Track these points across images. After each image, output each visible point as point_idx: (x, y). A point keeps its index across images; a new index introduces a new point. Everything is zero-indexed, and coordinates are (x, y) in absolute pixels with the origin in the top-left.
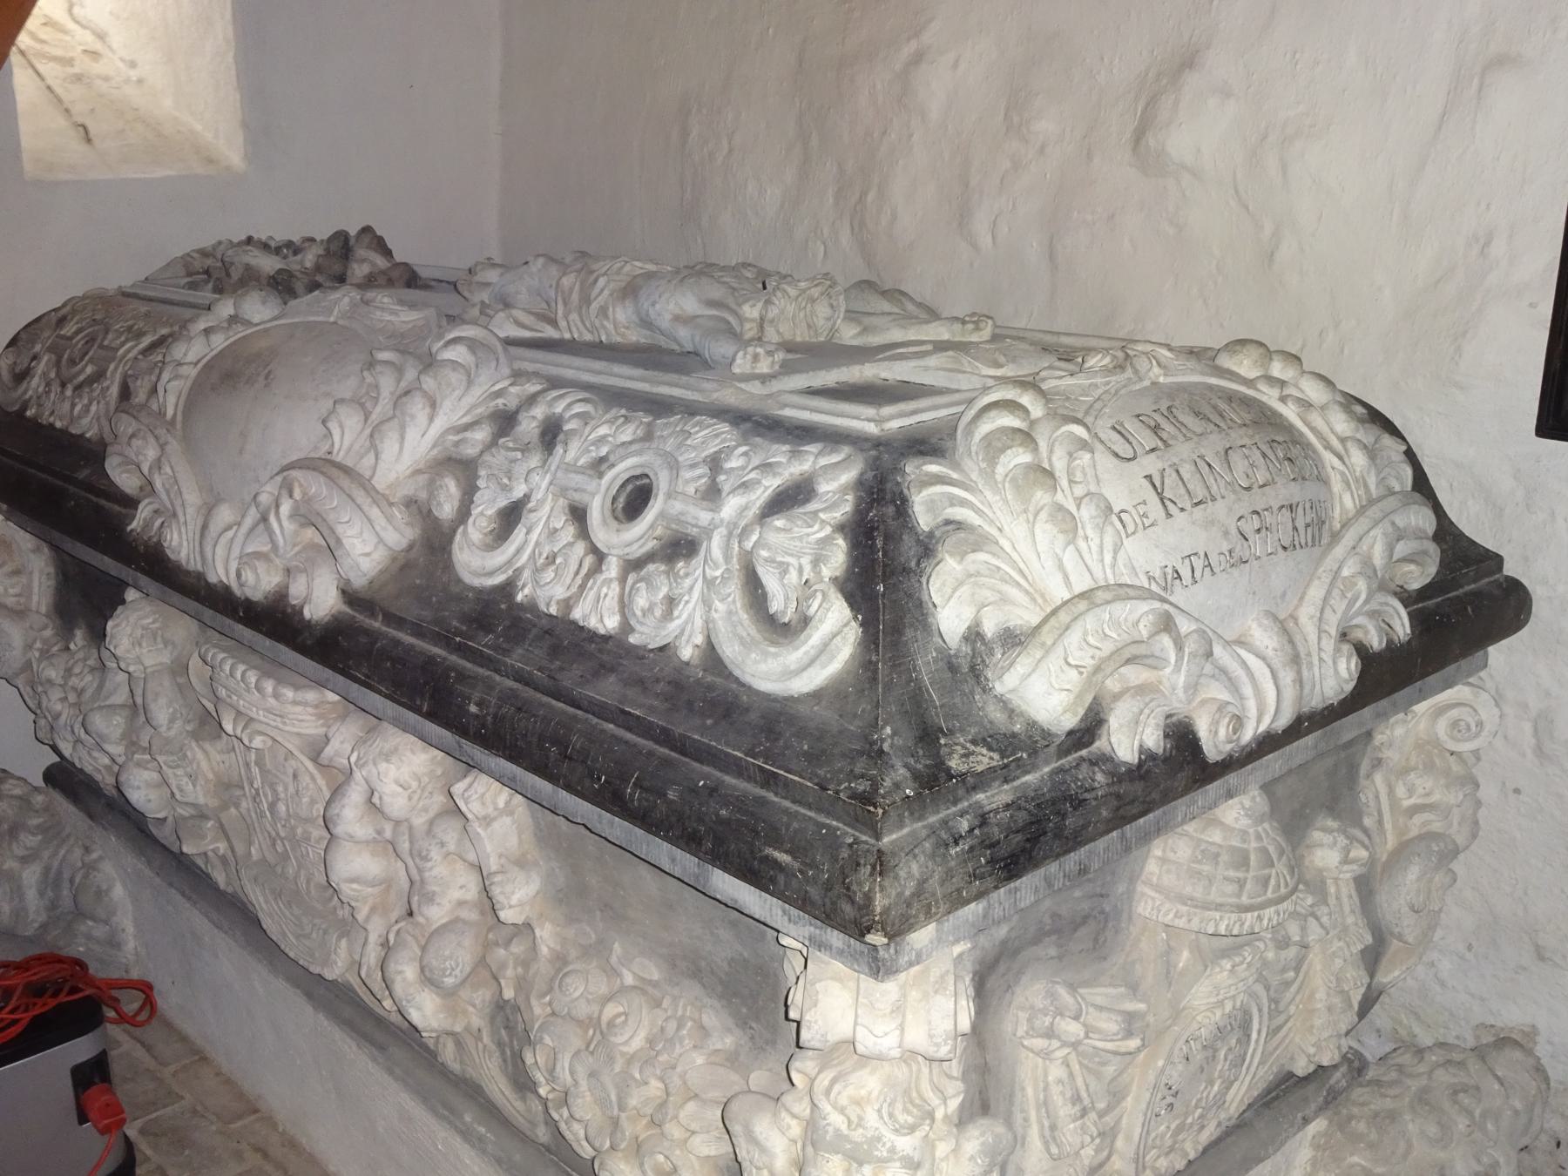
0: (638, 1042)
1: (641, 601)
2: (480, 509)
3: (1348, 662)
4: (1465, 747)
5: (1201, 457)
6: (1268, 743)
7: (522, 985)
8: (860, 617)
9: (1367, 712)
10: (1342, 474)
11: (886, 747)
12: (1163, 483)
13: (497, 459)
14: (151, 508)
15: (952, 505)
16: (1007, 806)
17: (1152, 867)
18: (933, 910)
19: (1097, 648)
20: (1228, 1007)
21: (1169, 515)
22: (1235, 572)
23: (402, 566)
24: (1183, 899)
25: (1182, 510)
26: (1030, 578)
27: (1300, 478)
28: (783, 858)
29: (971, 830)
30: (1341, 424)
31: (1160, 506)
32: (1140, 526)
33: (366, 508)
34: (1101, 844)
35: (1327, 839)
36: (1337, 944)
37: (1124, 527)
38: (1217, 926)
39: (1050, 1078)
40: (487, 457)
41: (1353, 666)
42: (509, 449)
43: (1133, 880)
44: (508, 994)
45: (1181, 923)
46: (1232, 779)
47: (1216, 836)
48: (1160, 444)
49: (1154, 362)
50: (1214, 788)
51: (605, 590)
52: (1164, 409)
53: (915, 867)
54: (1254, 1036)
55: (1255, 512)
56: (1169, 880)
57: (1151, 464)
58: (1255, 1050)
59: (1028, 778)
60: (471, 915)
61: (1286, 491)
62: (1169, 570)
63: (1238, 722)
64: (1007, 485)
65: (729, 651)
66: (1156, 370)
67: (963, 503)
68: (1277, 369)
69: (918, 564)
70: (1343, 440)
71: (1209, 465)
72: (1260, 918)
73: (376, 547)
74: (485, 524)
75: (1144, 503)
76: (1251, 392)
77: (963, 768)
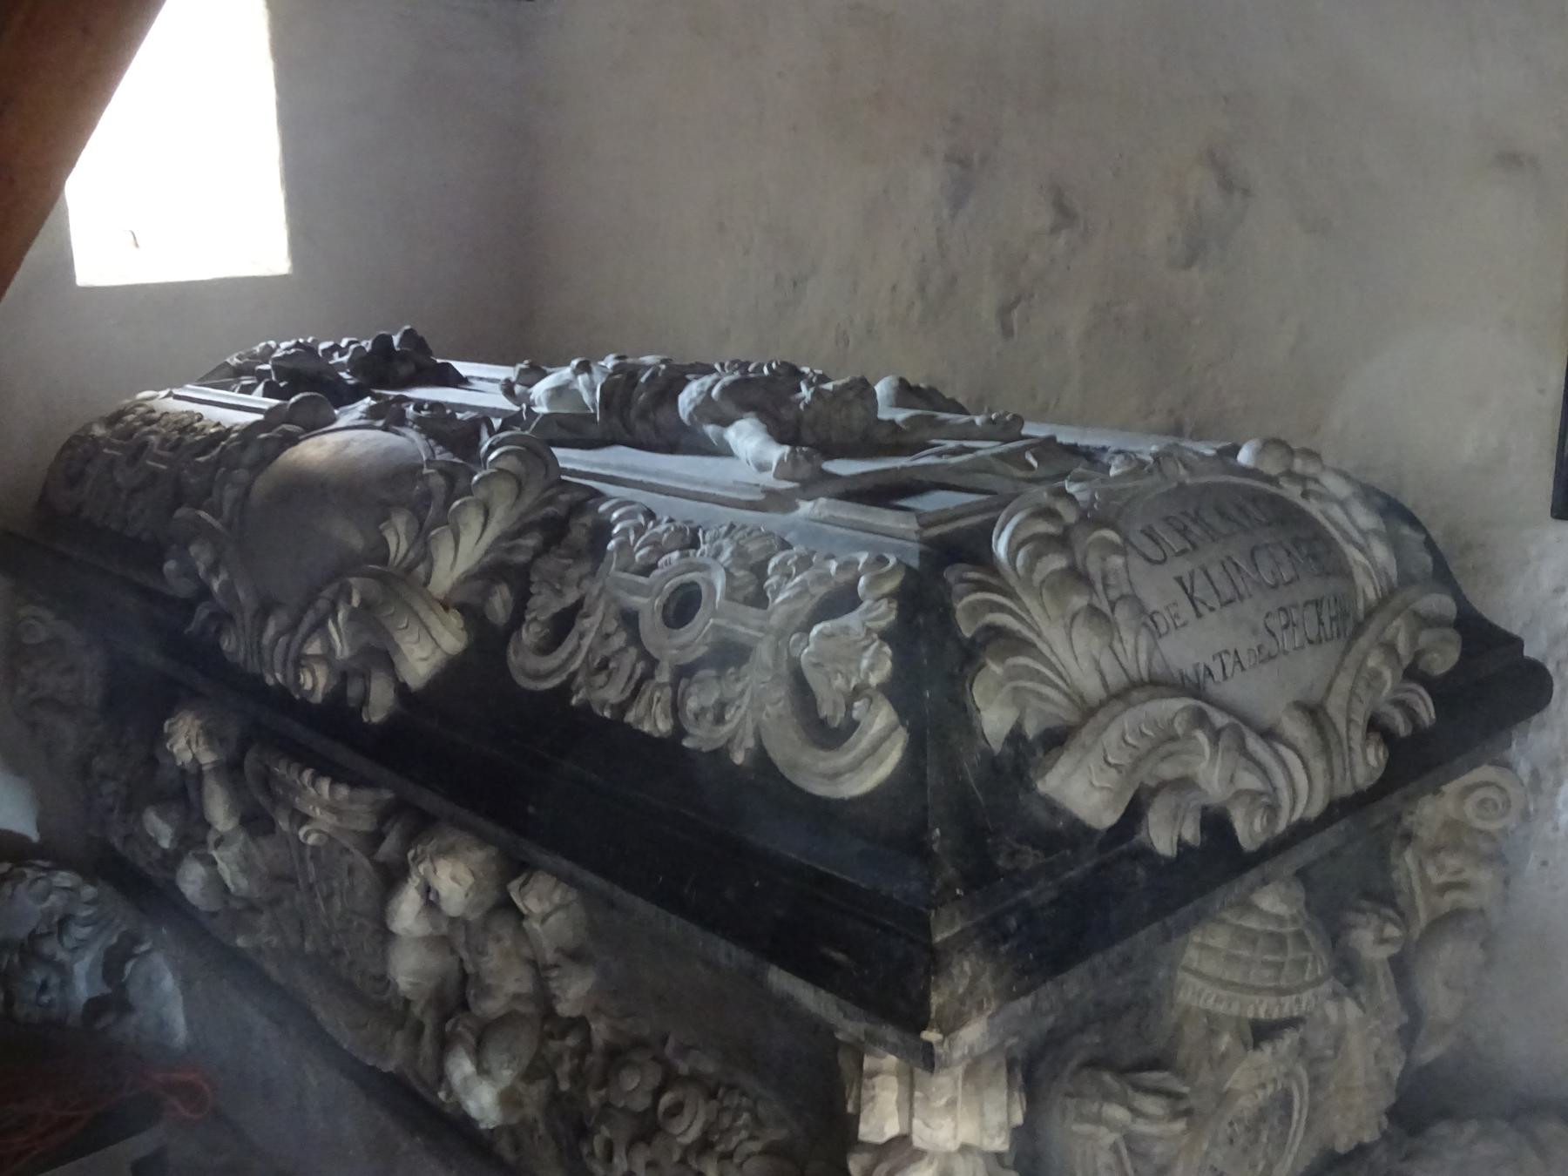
0: (694, 1133)
1: (692, 704)
2: (533, 615)
3: (1377, 750)
4: (1493, 826)
5: (1229, 558)
6: (1302, 831)
7: (577, 1076)
8: (907, 723)
9: (1396, 797)
10: (1365, 568)
11: (935, 847)
12: (1192, 587)
13: (549, 564)
14: (207, 611)
15: (992, 611)
16: (1053, 903)
17: (1192, 955)
18: (985, 1006)
19: (1134, 747)
20: (1270, 1089)
21: (1199, 615)
22: (1265, 668)
23: (453, 671)
24: (1226, 984)
25: (1212, 609)
26: (1069, 681)
27: (1326, 574)
28: (840, 957)
29: (1019, 927)
30: (1366, 519)
31: (1191, 608)
32: (1172, 625)
33: (422, 614)
34: (1142, 935)
35: (1361, 919)
36: (1375, 1023)
37: (1156, 627)
38: (1256, 1009)
39: (1099, 1165)
40: (539, 563)
41: (1381, 754)
42: (562, 557)
43: (1173, 967)
44: (565, 1086)
45: (1221, 1008)
46: (1268, 867)
47: (1252, 923)
48: (1189, 546)
49: (1180, 465)
50: (1252, 876)
51: (657, 694)
52: (1191, 511)
53: (967, 966)
54: (1295, 1116)
55: (1282, 609)
56: (1211, 967)
57: (1183, 567)
58: (1295, 1132)
59: (1072, 873)
60: (526, 1009)
61: (1311, 588)
62: (1202, 668)
63: (1273, 810)
64: (1044, 591)
65: (778, 755)
66: (1182, 472)
67: (1001, 608)
68: (1298, 465)
69: (961, 670)
70: (1363, 533)
71: (1236, 565)
72: (1298, 1001)
73: (433, 653)
74: (539, 629)
75: (1175, 604)
76: (1272, 489)
77: (1010, 867)
